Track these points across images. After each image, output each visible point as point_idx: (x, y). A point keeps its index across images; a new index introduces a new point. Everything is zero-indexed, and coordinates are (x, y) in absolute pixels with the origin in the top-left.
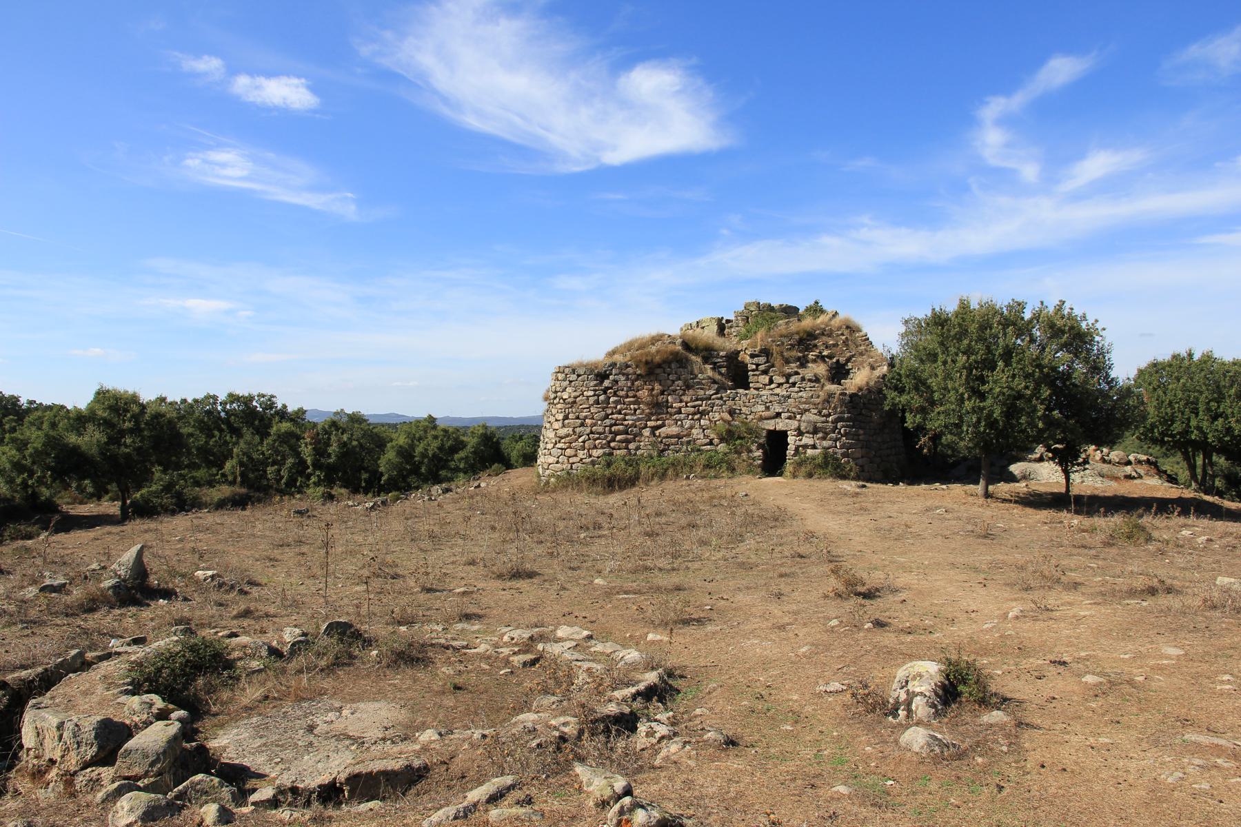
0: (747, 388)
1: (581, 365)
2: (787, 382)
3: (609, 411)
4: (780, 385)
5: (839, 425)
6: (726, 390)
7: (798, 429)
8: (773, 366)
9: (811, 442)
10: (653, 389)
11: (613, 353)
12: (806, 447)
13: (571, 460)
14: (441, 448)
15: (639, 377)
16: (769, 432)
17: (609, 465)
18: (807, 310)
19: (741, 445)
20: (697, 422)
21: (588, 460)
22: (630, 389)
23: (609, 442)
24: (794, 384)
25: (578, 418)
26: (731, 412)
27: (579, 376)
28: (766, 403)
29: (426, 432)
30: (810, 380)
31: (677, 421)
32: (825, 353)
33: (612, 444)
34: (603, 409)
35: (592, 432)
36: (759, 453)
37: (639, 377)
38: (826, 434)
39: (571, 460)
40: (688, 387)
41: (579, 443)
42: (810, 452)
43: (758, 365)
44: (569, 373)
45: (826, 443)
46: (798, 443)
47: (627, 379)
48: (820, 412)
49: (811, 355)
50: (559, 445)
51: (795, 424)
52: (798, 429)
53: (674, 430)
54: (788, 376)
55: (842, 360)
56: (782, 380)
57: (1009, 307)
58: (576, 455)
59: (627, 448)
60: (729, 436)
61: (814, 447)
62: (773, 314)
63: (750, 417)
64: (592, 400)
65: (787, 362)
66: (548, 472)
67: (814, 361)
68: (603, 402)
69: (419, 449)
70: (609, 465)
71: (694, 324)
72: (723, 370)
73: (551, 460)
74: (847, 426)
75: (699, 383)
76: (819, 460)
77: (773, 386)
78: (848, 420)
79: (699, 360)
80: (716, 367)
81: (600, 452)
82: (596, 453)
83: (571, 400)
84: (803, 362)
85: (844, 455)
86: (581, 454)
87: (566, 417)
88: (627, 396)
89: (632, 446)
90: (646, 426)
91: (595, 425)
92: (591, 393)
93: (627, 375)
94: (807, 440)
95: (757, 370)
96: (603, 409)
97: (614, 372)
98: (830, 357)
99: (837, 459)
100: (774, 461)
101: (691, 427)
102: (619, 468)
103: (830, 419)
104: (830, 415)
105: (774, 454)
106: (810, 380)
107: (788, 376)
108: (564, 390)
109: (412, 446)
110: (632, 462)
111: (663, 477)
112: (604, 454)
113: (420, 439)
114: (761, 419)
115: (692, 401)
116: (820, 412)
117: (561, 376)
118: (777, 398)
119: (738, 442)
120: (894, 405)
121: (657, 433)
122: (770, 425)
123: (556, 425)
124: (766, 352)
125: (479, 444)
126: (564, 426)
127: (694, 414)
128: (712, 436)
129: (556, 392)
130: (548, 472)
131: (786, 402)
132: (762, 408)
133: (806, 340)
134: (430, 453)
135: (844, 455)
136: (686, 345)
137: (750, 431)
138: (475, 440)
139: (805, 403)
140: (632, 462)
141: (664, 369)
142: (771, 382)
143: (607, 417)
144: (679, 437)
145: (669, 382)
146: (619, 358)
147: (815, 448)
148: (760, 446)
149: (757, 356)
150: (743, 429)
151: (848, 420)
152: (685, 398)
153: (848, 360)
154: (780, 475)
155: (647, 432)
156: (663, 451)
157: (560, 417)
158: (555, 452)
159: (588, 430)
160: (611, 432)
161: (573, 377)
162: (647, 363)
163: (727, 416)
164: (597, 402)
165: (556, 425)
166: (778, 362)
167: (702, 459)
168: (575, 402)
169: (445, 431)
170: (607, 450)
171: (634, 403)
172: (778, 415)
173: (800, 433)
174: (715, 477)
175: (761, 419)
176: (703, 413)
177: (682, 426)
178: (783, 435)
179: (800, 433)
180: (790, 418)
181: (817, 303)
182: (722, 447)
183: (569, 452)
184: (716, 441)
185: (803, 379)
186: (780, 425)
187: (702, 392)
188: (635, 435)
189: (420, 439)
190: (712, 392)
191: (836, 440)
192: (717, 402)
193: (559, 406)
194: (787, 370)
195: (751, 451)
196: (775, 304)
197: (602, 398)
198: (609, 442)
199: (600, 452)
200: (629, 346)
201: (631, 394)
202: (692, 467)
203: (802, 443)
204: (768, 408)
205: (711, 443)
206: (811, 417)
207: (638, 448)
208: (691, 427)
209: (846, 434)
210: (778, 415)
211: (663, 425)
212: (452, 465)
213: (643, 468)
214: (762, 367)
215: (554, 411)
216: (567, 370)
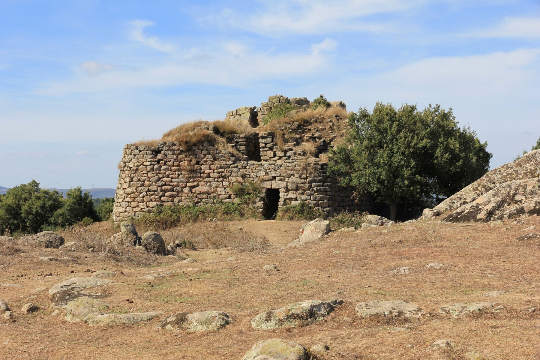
0: (259, 160)
1: (143, 144)
2: (285, 156)
3: (161, 176)
4: (280, 158)
5: (313, 185)
6: (240, 161)
7: (286, 187)
8: (276, 145)
10: (191, 161)
11: (168, 135)
12: (290, 199)
13: (135, 210)
14: (43, 207)
15: (182, 152)
17: (160, 212)
18: (316, 101)
19: (249, 198)
20: (219, 182)
21: (146, 209)
22: (175, 160)
23: (160, 197)
24: (289, 157)
25: (139, 180)
26: (243, 176)
27: (140, 151)
28: (274, 171)
29: (30, 194)
30: (299, 154)
31: (207, 182)
32: (316, 135)
33: (163, 199)
34: (157, 174)
35: (149, 190)
36: (260, 204)
37: (182, 152)
38: (305, 191)
39: (135, 210)
40: (215, 159)
41: (139, 199)
42: (294, 203)
43: (266, 144)
44: (134, 149)
45: (304, 197)
46: (286, 197)
47: (174, 154)
48: (300, 176)
49: (307, 136)
50: (126, 200)
51: (283, 184)
52: (286, 187)
53: (205, 189)
54: (285, 152)
55: (327, 140)
56: (282, 154)
57: (404, 110)
58: (138, 206)
59: (172, 201)
60: (241, 192)
61: (296, 199)
62: (288, 105)
64: (149, 168)
65: (286, 141)
66: (119, 218)
67: (308, 141)
68: (157, 169)
69: (25, 207)
70: (160, 212)
71: (234, 112)
72: (243, 147)
73: (121, 210)
74: (319, 186)
75: (222, 156)
76: (298, 209)
77: (276, 158)
78: (319, 181)
79: (224, 140)
80: (236, 146)
81: (154, 204)
82: (152, 204)
83: (134, 168)
84: (298, 142)
86: (141, 205)
87: (132, 180)
88: (173, 166)
89: (176, 200)
90: (186, 186)
91: (151, 185)
92: (149, 163)
93: (174, 150)
95: (265, 147)
96: (157, 174)
97: (164, 148)
98: (320, 138)
99: (310, 208)
100: (270, 209)
101: (217, 187)
102: (166, 215)
103: (307, 180)
104: (307, 178)
105: (271, 205)
106: (299, 154)
107: (285, 152)
108: (130, 161)
109: (19, 206)
110: (174, 210)
111: (196, 220)
112: (157, 205)
113: (25, 200)
114: (263, 181)
116: (300, 176)
117: (128, 151)
118: (273, 167)
120: (332, 171)
121: (193, 190)
122: (268, 185)
123: (125, 186)
124: (272, 135)
125: (74, 203)
126: (130, 186)
127: (219, 177)
128: (230, 193)
129: (125, 162)
130: (119, 218)
131: (282, 170)
132: (262, 173)
133: (303, 126)
134: (34, 211)
135: (316, 205)
136: (216, 130)
137: (255, 189)
138: (72, 200)
139: (292, 170)
140: (174, 210)
141: (197, 145)
142: (275, 155)
143: (159, 179)
144: (208, 193)
145: (202, 156)
146: (170, 140)
147: (296, 199)
148: (262, 199)
149: (266, 137)
150: (250, 187)
152: (213, 167)
153: (331, 140)
154: (274, 219)
155: (186, 190)
156: (198, 202)
157: (128, 180)
158: (124, 204)
159: (146, 189)
160: (162, 190)
161: (137, 152)
162: (186, 143)
163: (240, 179)
164: (153, 170)
165: (125, 186)
166: (279, 141)
168: (137, 170)
169: (46, 193)
170: (159, 203)
171: (178, 170)
172: (274, 178)
173: (287, 190)
174: (230, 220)
175: (263, 181)
177: (210, 186)
178: (277, 191)
179: (287, 190)
180: (281, 180)
181: (322, 97)
182: (237, 200)
183: (133, 204)
184: (233, 196)
185: (295, 154)
186: (275, 185)
187: (224, 163)
188: (179, 192)
189: (25, 200)
190: (231, 162)
191: (310, 195)
192: (234, 169)
193: (127, 172)
194: (285, 148)
195: (254, 203)
196: (291, 98)
197: (156, 166)
198: (160, 197)
199: (154, 204)
200: (179, 130)
201: (176, 164)
204: (267, 174)
205: (230, 197)
206: (295, 179)
207: (180, 201)
208: (217, 187)
209: (317, 191)
211: (198, 185)
212: (52, 220)
213: (182, 214)
214: (268, 146)
215: (124, 176)
216: (132, 147)
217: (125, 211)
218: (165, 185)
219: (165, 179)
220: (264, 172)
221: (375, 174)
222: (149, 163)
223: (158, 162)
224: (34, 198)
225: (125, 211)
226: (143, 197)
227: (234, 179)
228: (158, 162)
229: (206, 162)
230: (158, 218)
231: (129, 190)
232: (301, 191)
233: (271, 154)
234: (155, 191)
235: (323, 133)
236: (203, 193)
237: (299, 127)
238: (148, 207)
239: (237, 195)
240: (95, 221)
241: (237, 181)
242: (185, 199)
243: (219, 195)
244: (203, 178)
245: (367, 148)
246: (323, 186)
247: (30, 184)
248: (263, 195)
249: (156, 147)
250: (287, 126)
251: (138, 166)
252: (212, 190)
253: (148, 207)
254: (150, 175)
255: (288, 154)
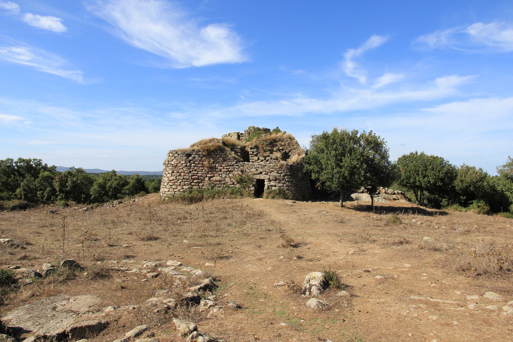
0: (249, 161)
1: (180, 150)
2: (265, 159)
4: (262, 161)
5: (285, 177)
6: (240, 162)
7: (269, 179)
8: (259, 153)
9: (274, 184)
10: (210, 161)
12: (272, 186)
13: (175, 190)
14: (118, 184)
15: (204, 156)
16: (257, 180)
17: (191, 192)
18: (274, 130)
19: (246, 185)
20: (228, 175)
22: (200, 161)
23: (191, 183)
24: (268, 160)
25: (178, 172)
26: (242, 171)
27: (179, 155)
29: (111, 177)
30: (274, 159)
32: (280, 148)
33: (192, 184)
34: (189, 169)
35: (184, 179)
36: (253, 188)
37: (204, 156)
38: (280, 181)
39: (175, 190)
40: (224, 160)
41: (178, 183)
42: (273, 188)
43: (253, 152)
44: (174, 153)
45: (280, 185)
47: (199, 157)
48: (278, 172)
49: (275, 149)
50: (170, 184)
51: (268, 177)
52: (269, 179)
53: (218, 178)
54: (265, 157)
55: (287, 151)
56: (263, 159)
58: (177, 188)
59: (198, 185)
60: (241, 181)
61: (275, 186)
63: (250, 174)
64: (184, 165)
65: (265, 151)
66: (165, 195)
67: (276, 151)
69: (108, 184)
70: (191, 192)
71: (228, 135)
72: (239, 154)
73: (166, 190)
75: (229, 159)
76: (277, 192)
78: (289, 175)
79: (229, 149)
80: (236, 153)
81: (187, 187)
82: (185, 187)
83: (175, 165)
84: (272, 152)
85: (287, 190)
86: (179, 188)
87: (173, 172)
88: (199, 164)
89: (200, 185)
90: (206, 177)
91: (185, 175)
94: (272, 183)
95: (253, 154)
96: (189, 169)
97: (194, 153)
98: (283, 150)
99: (284, 191)
100: (259, 192)
101: (225, 177)
102: (195, 194)
104: (282, 173)
105: (259, 189)
106: (274, 159)
107: (265, 157)
108: (172, 161)
109: (105, 183)
111: (213, 198)
112: (189, 188)
113: (109, 180)
114: (254, 174)
115: (226, 166)
116: (278, 172)
117: (171, 155)
118: (260, 166)
119: (245, 183)
120: (307, 170)
121: (211, 179)
122: (258, 177)
123: (169, 175)
124: (256, 147)
125: (135, 183)
126: (172, 176)
127: (227, 172)
128: (234, 181)
129: (169, 161)
130: (165, 195)
132: (254, 170)
133: (273, 143)
135: (287, 190)
136: (224, 143)
137: (249, 179)
138: (133, 181)
140: (201, 191)
141: (215, 153)
142: (258, 159)
143: (190, 172)
144: (220, 181)
146: (196, 148)
147: (276, 186)
148: (254, 186)
149: (253, 148)
150: (247, 178)
151: (289, 175)
152: (223, 165)
153: (290, 151)
155: (207, 179)
156: (213, 187)
157: (170, 172)
158: (168, 186)
159: (182, 178)
160: (192, 179)
161: (176, 155)
162: (207, 150)
163: (240, 173)
164: (186, 166)
167: (230, 191)
168: (177, 166)
169: (120, 177)
170: (190, 186)
172: (261, 173)
173: (270, 180)
175: (254, 174)
176: (230, 172)
177: (221, 177)
178: (263, 181)
179: (270, 180)
180: (265, 174)
182: (238, 186)
184: (235, 183)
185: (271, 158)
186: (262, 177)
187: (230, 163)
188: (202, 180)
189: (109, 180)
192: (236, 167)
193: (170, 167)
194: (265, 155)
196: (261, 127)
197: (188, 164)
198: (191, 183)
199: (187, 187)
200: (200, 143)
201: (200, 163)
202: (225, 194)
203: (270, 184)
204: (257, 170)
205: (233, 184)
206: (274, 174)
207: (203, 186)
208: (225, 177)
209: (288, 181)
210: (261, 173)
213: (205, 194)
214: (255, 153)
215: (168, 169)
217: (169, 191)
218: (194, 175)
219: (194, 172)
220: (255, 168)
221: (341, 172)
222: (184, 162)
223: (190, 161)
224: (113, 180)
225: (169, 191)
226: (180, 183)
227: (236, 173)
228: (190, 162)
229: (219, 162)
230: (190, 196)
231: (171, 178)
232: (278, 181)
233: (256, 158)
234: (187, 179)
235: (284, 147)
236: (217, 181)
237: (271, 143)
238: (183, 189)
239: (238, 183)
240: (147, 193)
241: (238, 174)
242: (206, 184)
243: (227, 183)
244: (217, 172)
245: (334, 156)
246: (291, 178)
247: (111, 172)
248: (254, 183)
249: (188, 152)
250: (264, 142)
251: (177, 164)
253: (183, 189)
254: (184, 169)
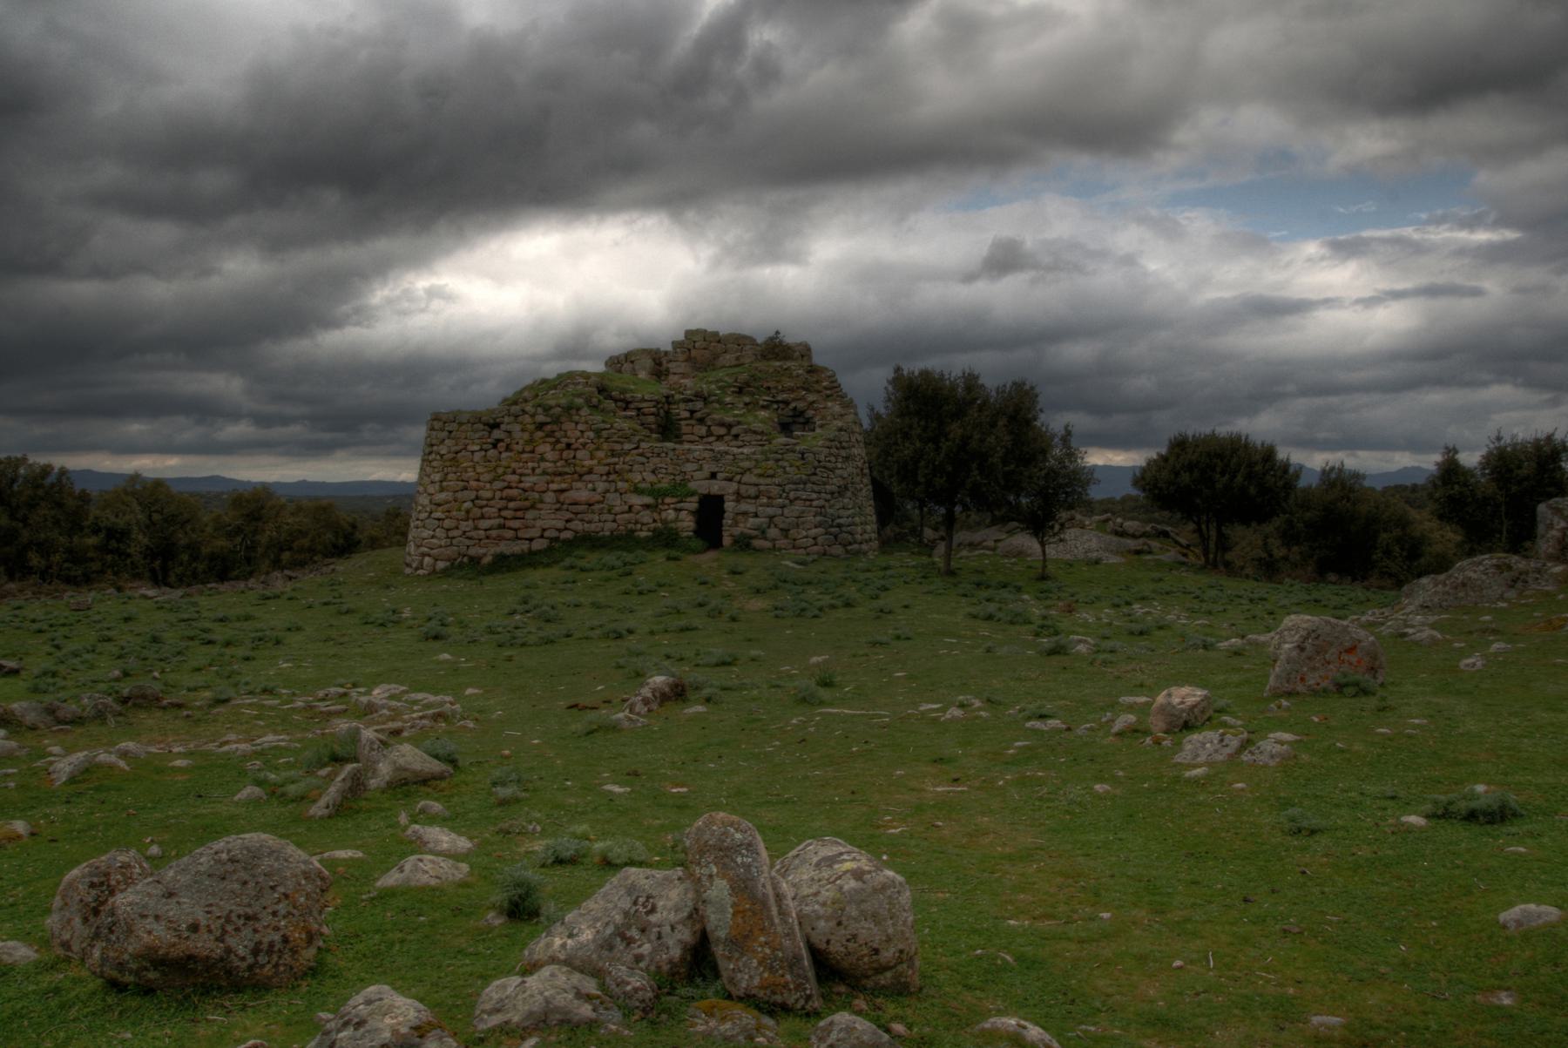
12: (745, 513)
24: (736, 436)
43: (692, 412)
45: (770, 511)
51: (734, 486)
95: (691, 418)
127: (608, 474)
142: (710, 434)
178: (719, 499)
214: (698, 415)
233: (703, 430)
252: (598, 498)
255: (734, 431)
